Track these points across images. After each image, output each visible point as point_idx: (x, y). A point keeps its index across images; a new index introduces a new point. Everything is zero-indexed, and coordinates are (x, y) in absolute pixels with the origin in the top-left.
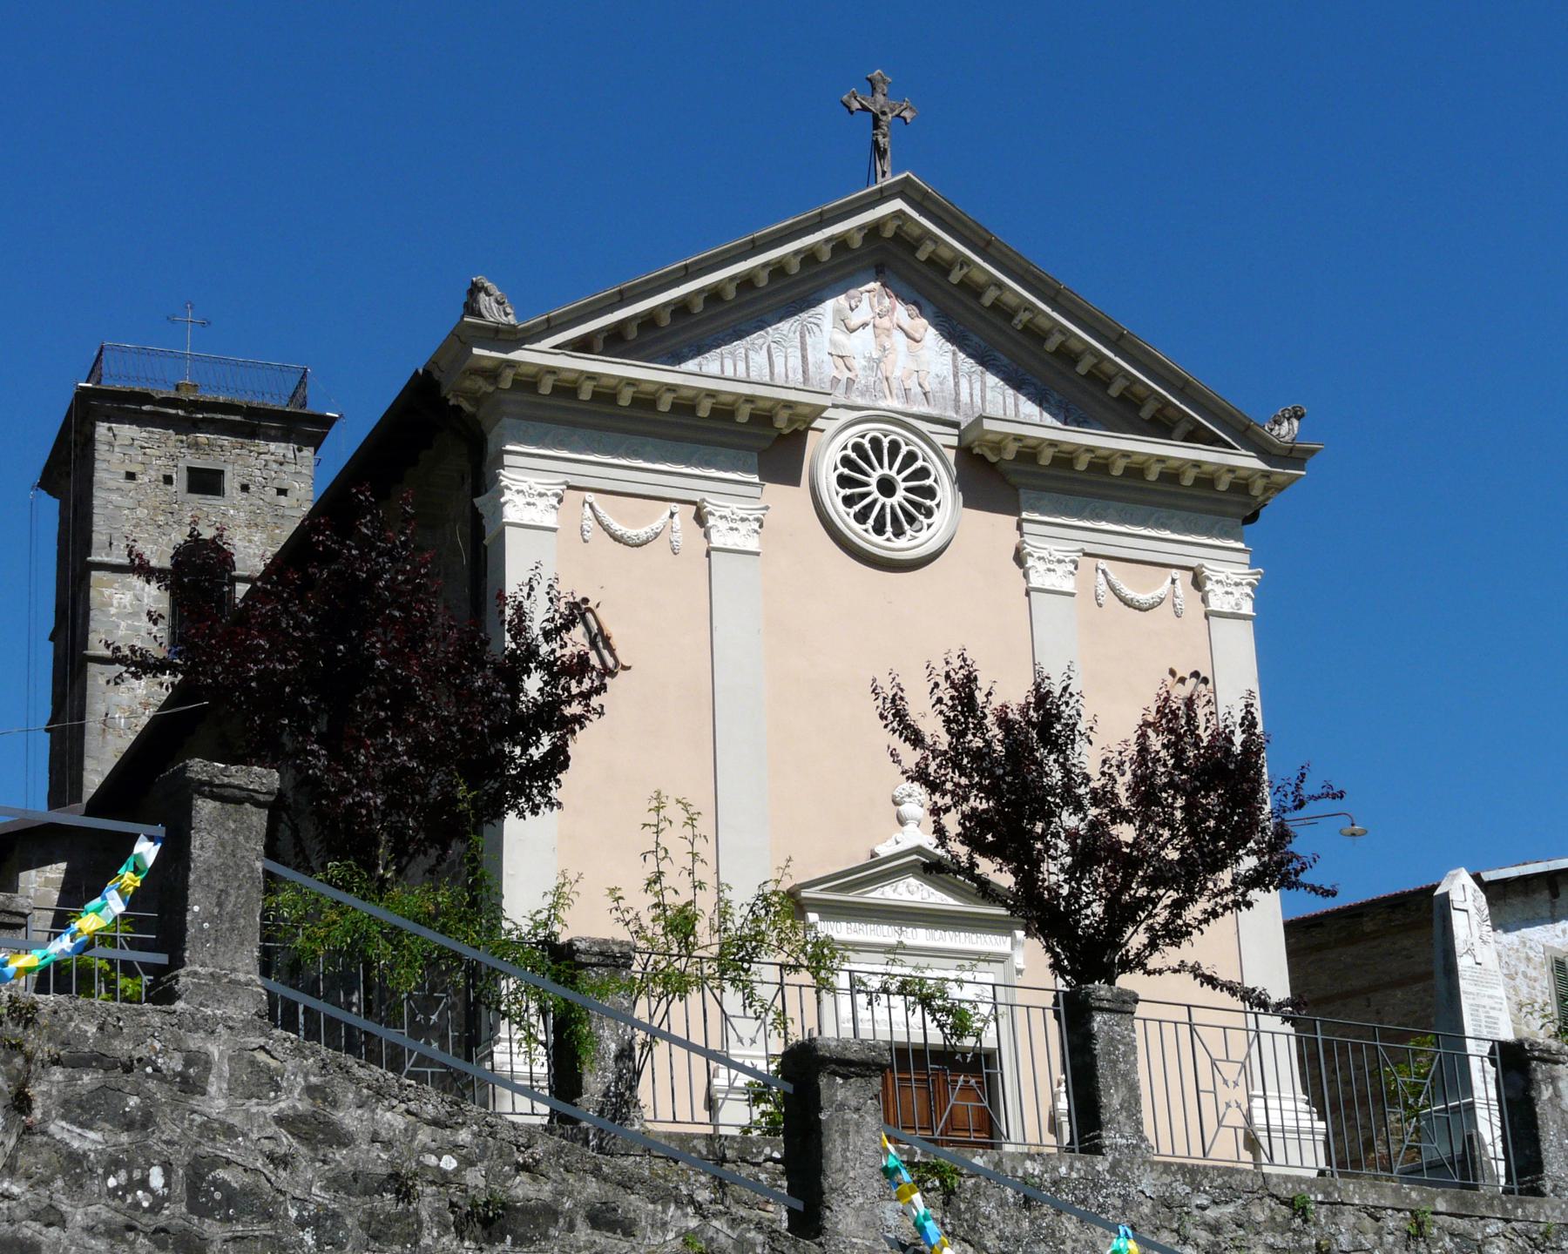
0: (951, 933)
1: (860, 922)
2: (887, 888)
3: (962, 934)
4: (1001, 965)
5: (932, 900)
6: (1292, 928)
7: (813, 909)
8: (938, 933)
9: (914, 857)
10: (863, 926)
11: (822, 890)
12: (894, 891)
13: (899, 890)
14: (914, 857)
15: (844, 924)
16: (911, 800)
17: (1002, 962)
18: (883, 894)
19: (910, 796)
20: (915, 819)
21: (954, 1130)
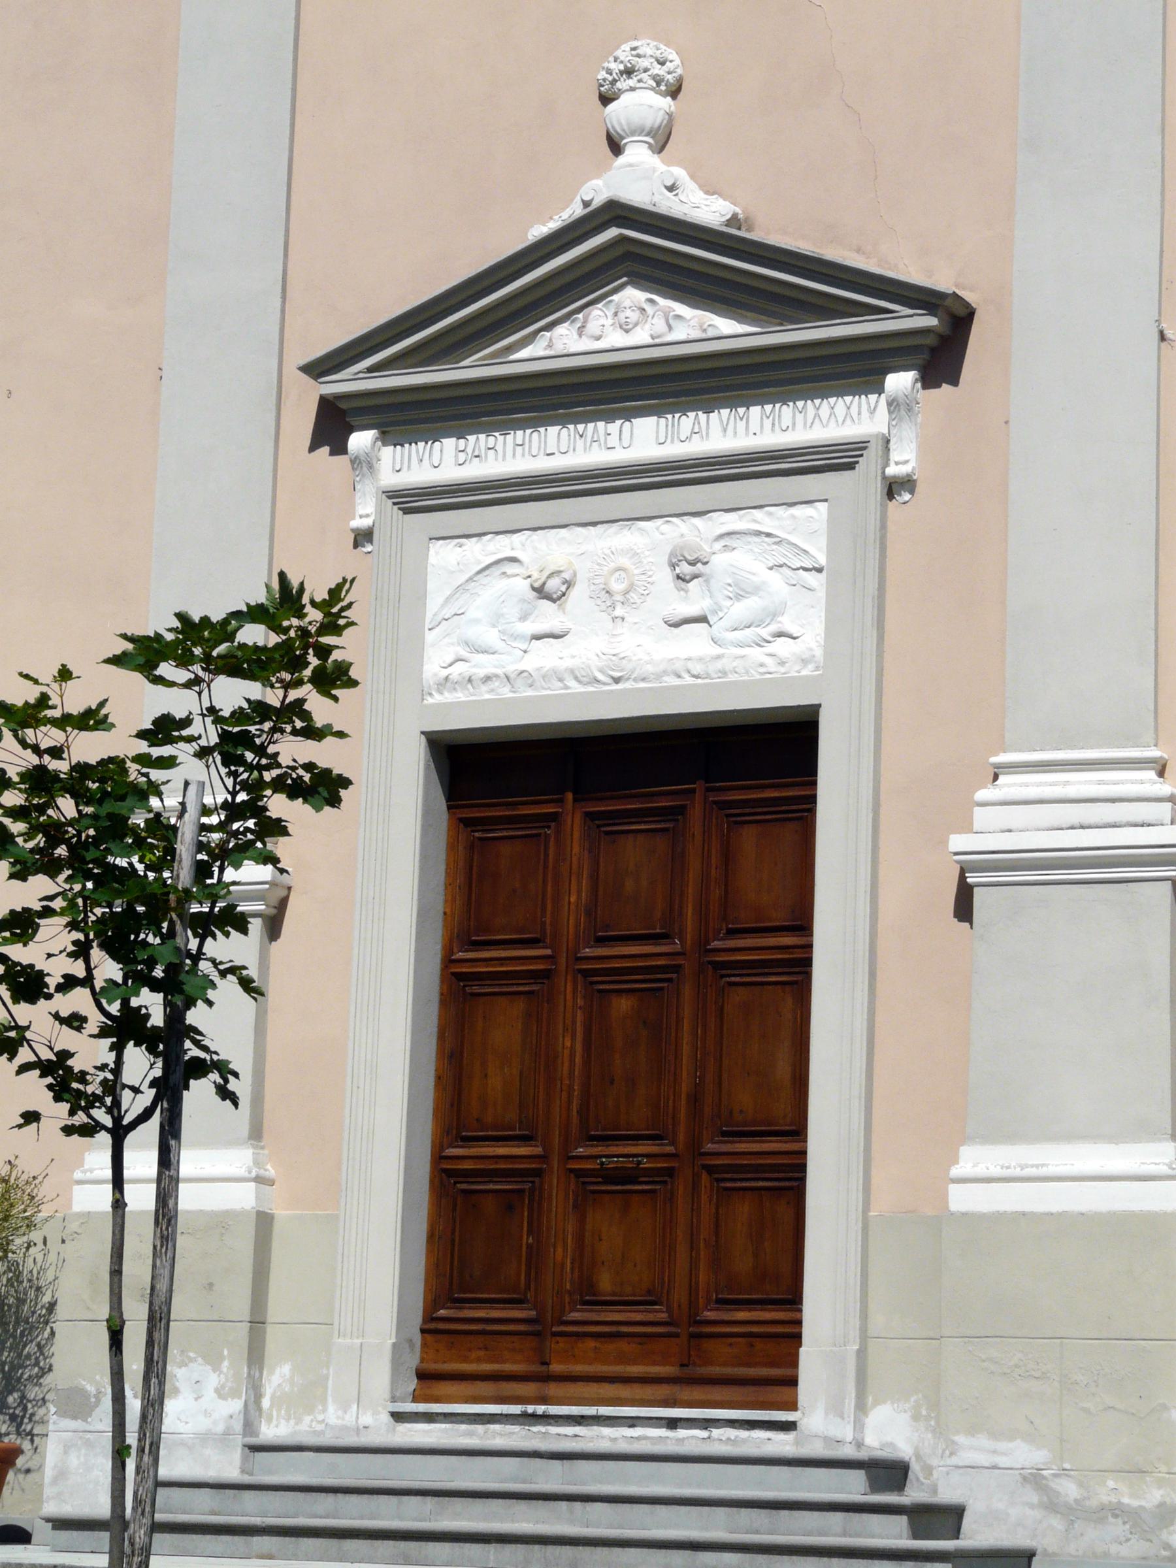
0: (725, 412)
1: (488, 429)
2: (562, 330)
3: (755, 410)
4: (846, 474)
5: (679, 334)
6: (253, 1153)
7: (365, 420)
8: (687, 421)
9: (612, 233)
10: (497, 440)
11: (370, 370)
12: (581, 331)
13: (593, 327)
14: (612, 233)
15: (449, 443)
16: (632, 82)
17: (851, 467)
18: (550, 346)
19: (629, 72)
20: (640, 131)
21: (731, 933)
